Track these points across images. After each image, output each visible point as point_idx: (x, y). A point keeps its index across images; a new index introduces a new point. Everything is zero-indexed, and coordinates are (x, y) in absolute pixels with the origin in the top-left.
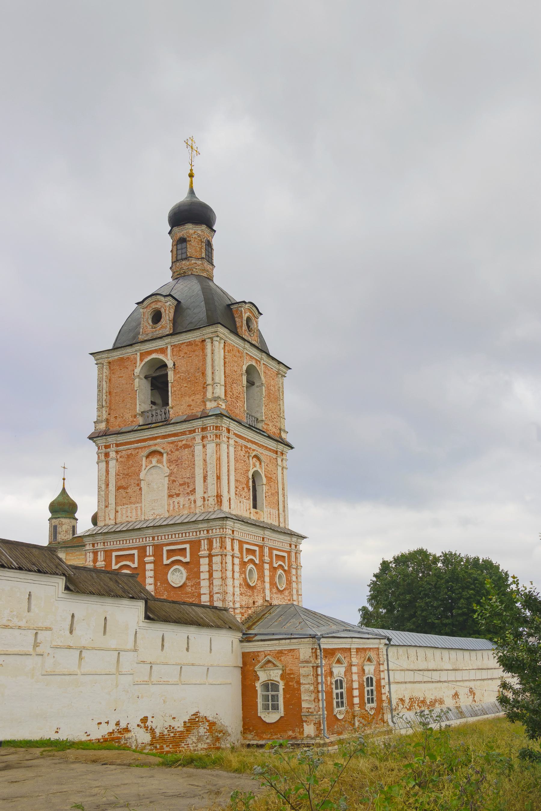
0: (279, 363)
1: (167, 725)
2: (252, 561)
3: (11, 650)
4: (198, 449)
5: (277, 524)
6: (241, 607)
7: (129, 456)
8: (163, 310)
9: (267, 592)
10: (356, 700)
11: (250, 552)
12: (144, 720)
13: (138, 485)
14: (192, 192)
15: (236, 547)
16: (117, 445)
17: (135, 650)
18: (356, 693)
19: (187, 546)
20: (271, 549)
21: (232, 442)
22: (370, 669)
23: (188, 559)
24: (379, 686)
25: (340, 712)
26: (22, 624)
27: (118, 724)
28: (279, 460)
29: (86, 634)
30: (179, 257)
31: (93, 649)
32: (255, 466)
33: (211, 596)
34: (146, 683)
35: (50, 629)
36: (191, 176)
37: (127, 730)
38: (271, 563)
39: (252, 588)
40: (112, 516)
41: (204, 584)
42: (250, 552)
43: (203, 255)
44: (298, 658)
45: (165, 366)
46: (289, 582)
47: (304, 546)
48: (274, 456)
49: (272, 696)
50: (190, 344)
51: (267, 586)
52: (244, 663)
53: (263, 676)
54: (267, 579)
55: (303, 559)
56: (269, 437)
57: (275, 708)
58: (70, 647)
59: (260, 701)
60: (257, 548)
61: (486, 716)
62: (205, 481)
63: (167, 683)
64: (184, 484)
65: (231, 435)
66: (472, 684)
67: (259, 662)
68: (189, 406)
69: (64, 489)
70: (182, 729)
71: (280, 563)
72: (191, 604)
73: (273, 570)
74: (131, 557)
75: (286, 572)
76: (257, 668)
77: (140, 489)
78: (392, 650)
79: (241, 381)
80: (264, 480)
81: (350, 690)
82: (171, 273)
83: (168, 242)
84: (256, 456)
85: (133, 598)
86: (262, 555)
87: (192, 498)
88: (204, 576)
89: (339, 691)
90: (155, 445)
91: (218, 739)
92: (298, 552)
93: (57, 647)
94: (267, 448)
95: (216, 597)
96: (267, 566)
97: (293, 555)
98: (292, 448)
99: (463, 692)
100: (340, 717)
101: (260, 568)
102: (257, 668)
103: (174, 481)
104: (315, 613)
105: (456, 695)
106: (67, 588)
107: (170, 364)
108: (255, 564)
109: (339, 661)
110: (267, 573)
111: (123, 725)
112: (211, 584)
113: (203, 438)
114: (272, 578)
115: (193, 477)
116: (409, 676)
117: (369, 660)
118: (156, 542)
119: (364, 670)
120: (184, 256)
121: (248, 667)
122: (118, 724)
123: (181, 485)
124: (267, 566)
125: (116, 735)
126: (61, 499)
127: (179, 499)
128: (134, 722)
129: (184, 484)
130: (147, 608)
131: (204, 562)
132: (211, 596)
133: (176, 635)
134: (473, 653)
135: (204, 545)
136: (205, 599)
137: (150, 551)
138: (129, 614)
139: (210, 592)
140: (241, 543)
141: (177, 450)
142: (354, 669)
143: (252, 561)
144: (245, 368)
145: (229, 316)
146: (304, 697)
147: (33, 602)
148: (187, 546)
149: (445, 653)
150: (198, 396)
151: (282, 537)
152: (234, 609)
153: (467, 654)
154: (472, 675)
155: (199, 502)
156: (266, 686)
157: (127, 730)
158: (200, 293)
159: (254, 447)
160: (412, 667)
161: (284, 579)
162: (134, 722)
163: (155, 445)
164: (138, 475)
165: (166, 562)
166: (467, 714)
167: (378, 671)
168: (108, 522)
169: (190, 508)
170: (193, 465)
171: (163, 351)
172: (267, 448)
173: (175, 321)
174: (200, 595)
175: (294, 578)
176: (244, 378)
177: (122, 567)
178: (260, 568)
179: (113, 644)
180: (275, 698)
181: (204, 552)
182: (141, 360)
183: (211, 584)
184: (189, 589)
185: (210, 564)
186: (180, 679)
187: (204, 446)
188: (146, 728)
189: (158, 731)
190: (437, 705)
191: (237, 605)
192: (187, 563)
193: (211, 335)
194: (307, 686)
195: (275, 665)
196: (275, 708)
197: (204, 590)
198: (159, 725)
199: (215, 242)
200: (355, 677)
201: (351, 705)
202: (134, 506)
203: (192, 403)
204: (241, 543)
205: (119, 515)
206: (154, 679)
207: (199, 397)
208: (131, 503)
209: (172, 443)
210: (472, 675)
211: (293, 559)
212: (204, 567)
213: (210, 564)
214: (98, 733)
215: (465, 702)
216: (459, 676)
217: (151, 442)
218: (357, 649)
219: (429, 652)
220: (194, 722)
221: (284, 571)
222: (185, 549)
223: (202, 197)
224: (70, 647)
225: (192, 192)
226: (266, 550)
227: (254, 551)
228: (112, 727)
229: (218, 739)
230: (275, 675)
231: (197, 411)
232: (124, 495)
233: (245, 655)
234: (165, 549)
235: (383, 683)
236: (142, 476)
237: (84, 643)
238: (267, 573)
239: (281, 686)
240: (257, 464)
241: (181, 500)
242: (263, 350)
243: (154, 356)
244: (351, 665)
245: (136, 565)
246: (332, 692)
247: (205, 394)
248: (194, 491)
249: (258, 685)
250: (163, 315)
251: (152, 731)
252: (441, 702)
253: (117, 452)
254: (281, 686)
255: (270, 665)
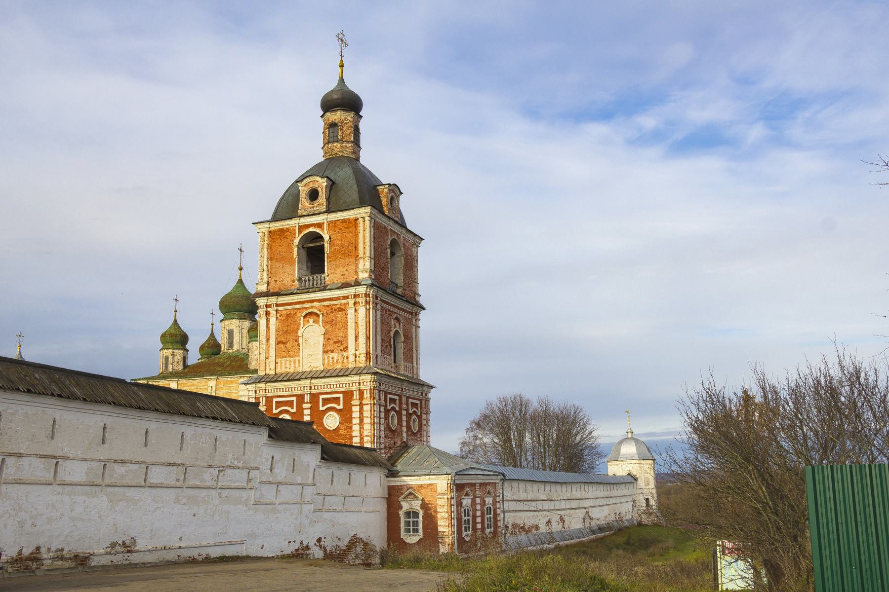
0: (415, 235)
1: (334, 544)
2: (393, 409)
3: (233, 485)
4: (351, 312)
5: (410, 375)
6: (385, 447)
7: (288, 316)
8: (320, 190)
9: (405, 435)
10: (479, 526)
11: (393, 401)
12: (319, 540)
13: (296, 341)
14: (342, 80)
15: (382, 397)
16: (277, 305)
17: (314, 485)
18: (479, 520)
19: (341, 395)
20: (408, 398)
21: (379, 307)
22: (489, 500)
23: (341, 407)
24: (495, 515)
25: (467, 535)
26: (240, 465)
27: (301, 543)
28: (414, 320)
29: (281, 472)
30: (331, 140)
31: (286, 484)
32: (395, 327)
33: (362, 439)
34: (320, 511)
35: (257, 468)
36: (342, 66)
37: (307, 548)
38: (407, 410)
39: (393, 431)
40: (273, 367)
41: (356, 428)
42: (393, 401)
43: (352, 139)
44: (436, 491)
45: (320, 237)
46: (421, 426)
47: (432, 394)
48: (410, 316)
49: (413, 522)
50: (344, 221)
51: (405, 429)
52: (389, 494)
53: (405, 506)
54: (404, 424)
55: (432, 404)
56: (407, 301)
57: (416, 531)
58: (270, 483)
59: (402, 525)
60: (397, 398)
61: (572, 541)
62: (356, 340)
63: (335, 511)
64: (338, 342)
65: (378, 301)
66: (562, 513)
67: (402, 494)
68: (344, 275)
69: (175, 320)
70: (344, 548)
71: (414, 409)
72: (345, 445)
73: (409, 415)
74: (290, 404)
75: (420, 417)
76: (400, 499)
77: (298, 345)
78: (506, 484)
79: (386, 253)
80: (402, 338)
81: (474, 517)
82: (322, 153)
83: (320, 125)
84: (397, 318)
85: (314, 443)
86: (401, 404)
87: (345, 354)
88: (356, 421)
89: (466, 518)
90: (312, 307)
91: (370, 556)
92: (427, 400)
93: (264, 483)
94: (404, 310)
95: (366, 439)
96: (404, 412)
97: (424, 402)
98: (424, 309)
99: (555, 518)
100: (467, 539)
101: (399, 414)
102: (400, 499)
103: (329, 339)
104: (445, 453)
105: (549, 523)
106: (270, 436)
107: (326, 237)
108: (396, 411)
109: (467, 495)
110: (404, 418)
111: (305, 544)
112: (361, 428)
113: (355, 303)
114: (408, 422)
115: (346, 336)
116: (520, 506)
117: (489, 493)
118: (313, 391)
119: (484, 501)
120: (335, 139)
121: (393, 497)
122: (301, 543)
123: (335, 343)
124: (404, 412)
125: (301, 552)
126: (173, 331)
127: (331, 355)
128: (312, 542)
129: (338, 342)
130: (323, 452)
131: (356, 409)
132: (362, 439)
133: (341, 472)
134: (564, 487)
135: (356, 395)
136: (356, 441)
137: (307, 398)
138: (310, 457)
139: (361, 435)
140: (386, 393)
141: (332, 312)
142: (478, 500)
143: (393, 409)
144: (389, 242)
145: (370, 192)
146: (440, 522)
147: (247, 448)
148: (341, 395)
149: (542, 486)
150: (351, 267)
151: (416, 387)
152: (380, 449)
153: (559, 486)
154: (563, 505)
155: (352, 358)
156: (408, 514)
157: (307, 548)
158: (352, 175)
159: (395, 310)
160: (515, 498)
161: (417, 423)
162: (312, 542)
163: (312, 307)
164: (297, 332)
165: (321, 408)
166: (558, 539)
167: (495, 503)
168: (268, 372)
169: (343, 363)
170: (346, 326)
171: (320, 225)
172: (404, 310)
173: (328, 199)
174: (351, 437)
175: (424, 422)
176: (389, 251)
177: (281, 412)
178: (399, 414)
179: (299, 479)
180: (416, 523)
181: (355, 402)
182: (300, 232)
183: (361, 428)
184: (342, 432)
185: (361, 410)
186: (55, 477)
187: (356, 310)
188: (320, 546)
189: (328, 549)
190: (533, 531)
191: (383, 446)
192: (340, 410)
193: (363, 215)
194: (443, 514)
195: (416, 497)
196: (416, 531)
197: (356, 433)
198: (329, 544)
199: (362, 125)
200: (478, 507)
201: (475, 529)
202: (292, 359)
203: (345, 273)
204: (386, 393)
205: (278, 366)
206: (326, 507)
207: (352, 267)
208: (290, 356)
209: (328, 306)
210: (563, 505)
211: (424, 406)
212: (356, 415)
213: (361, 410)
214: (289, 550)
215: (556, 527)
216: (552, 505)
217: (309, 305)
218: (480, 484)
219: (529, 485)
220: (354, 541)
221: (417, 416)
222: (339, 398)
223: (353, 85)
224: (270, 483)
225: (342, 80)
226: (404, 399)
227: (395, 400)
228: (297, 546)
229: (370, 556)
230: (416, 505)
231: (351, 280)
232: (284, 349)
233: (389, 487)
234: (321, 397)
235: (499, 511)
236: (300, 333)
237: (280, 479)
238: (404, 418)
239: (421, 515)
240: (397, 325)
241: (335, 355)
242: (403, 225)
243: (311, 229)
244: (475, 497)
245: (294, 410)
246: (461, 519)
247: (357, 265)
248: (346, 348)
249: (401, 513)
250: (320, 193)
251: (325, 551)
252: (537, 528)
253: (277, 311)
254: (421, 515)
255: (412, 496)
